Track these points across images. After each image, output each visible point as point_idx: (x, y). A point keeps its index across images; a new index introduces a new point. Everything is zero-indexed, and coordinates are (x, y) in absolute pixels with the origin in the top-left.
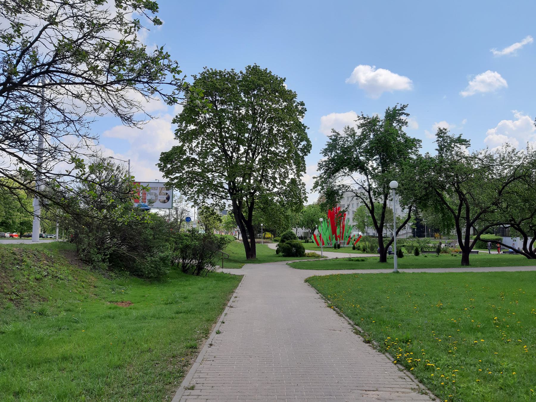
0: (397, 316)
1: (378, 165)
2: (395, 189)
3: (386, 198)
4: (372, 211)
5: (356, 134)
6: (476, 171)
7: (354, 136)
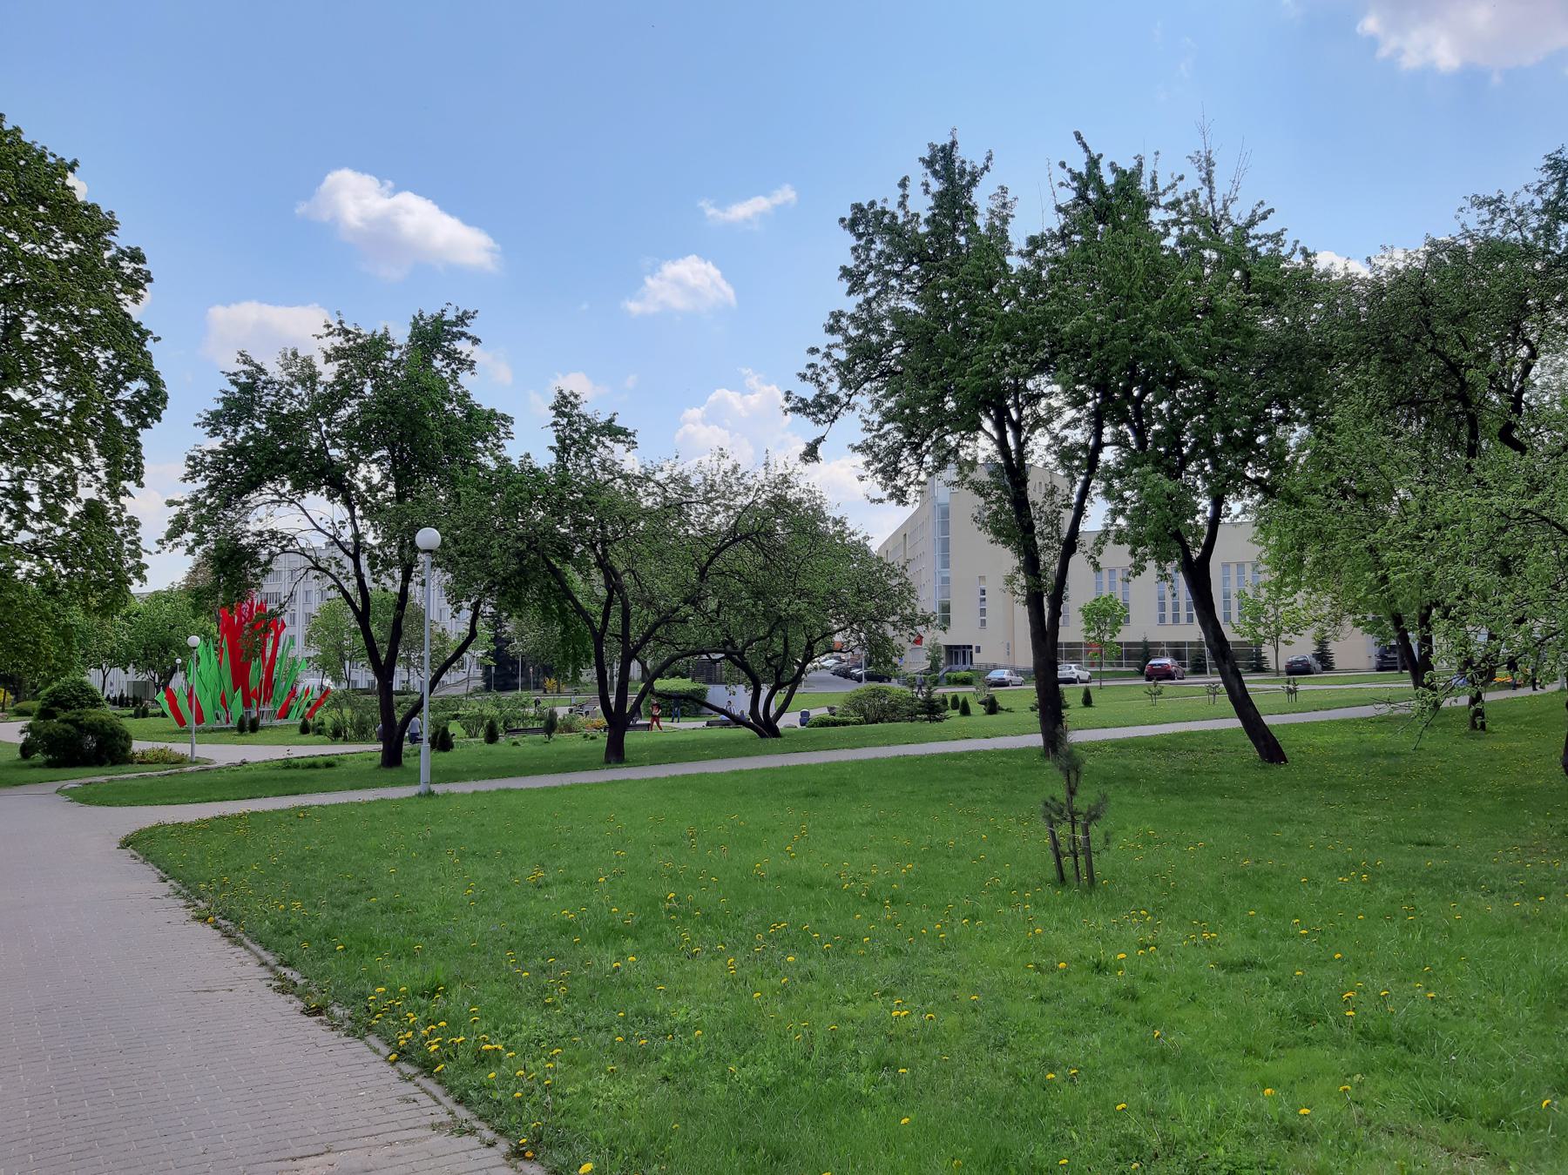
0: (415, 922)
1: (386, 476)
2: (430, 551)
3: (407, 578)
4: (363, 617)
5: (321, 378)
6: (647, 513)
7: (314, 384)
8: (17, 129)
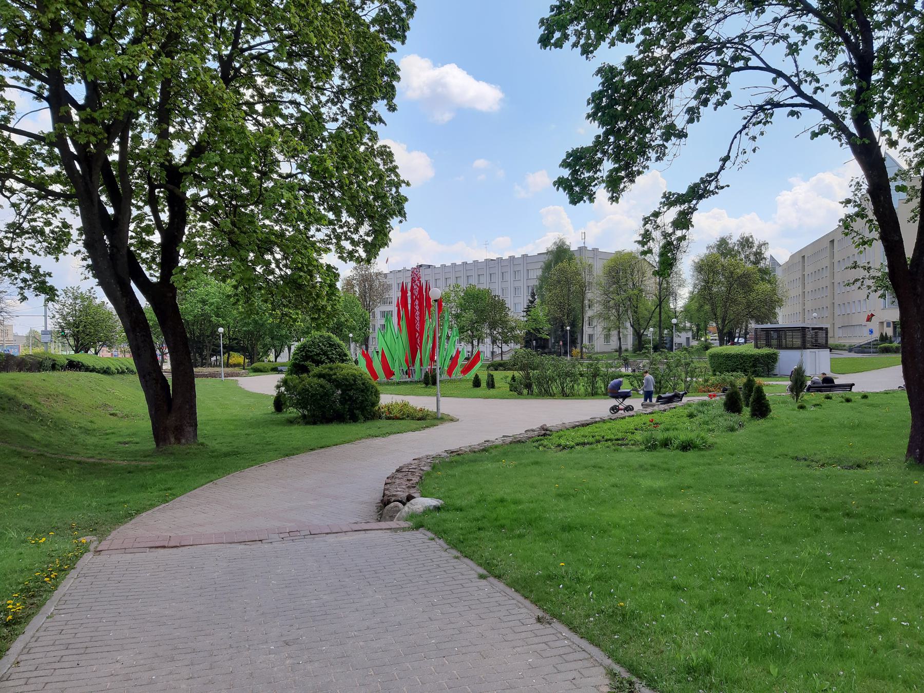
8: (542, 22)
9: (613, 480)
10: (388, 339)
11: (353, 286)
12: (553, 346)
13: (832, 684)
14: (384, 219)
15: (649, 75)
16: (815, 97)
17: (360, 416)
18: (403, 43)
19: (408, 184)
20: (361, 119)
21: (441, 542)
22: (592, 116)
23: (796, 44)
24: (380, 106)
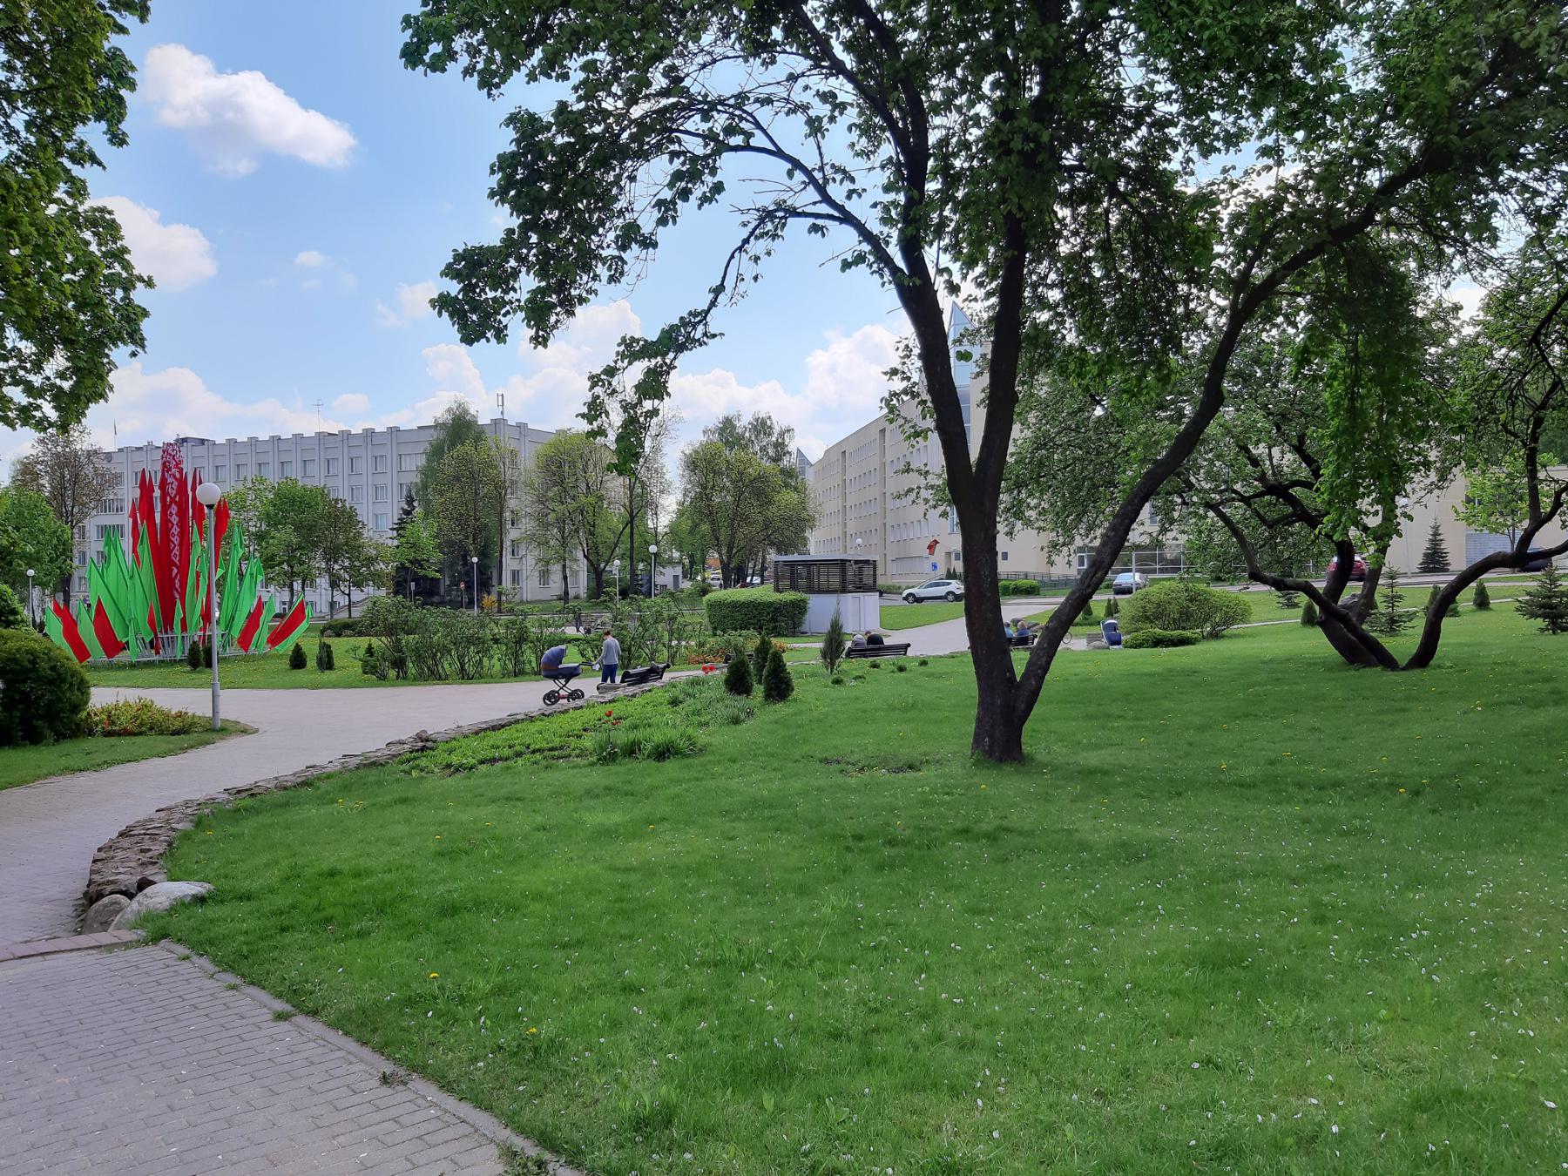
9: (539, 819)
10: (113, 576)
11: (36, 476)
12: (449, 591)
13: (853, 1111)
14: (97, 347)
15: (595, 137)
16: (849, 206)
17: (47, 732)
18: (143, 19)
19: (149, 283)
20: (51, 152)
21: (204, 962)
22: (500, 194)
23: (819, 119)
24: (92, 133)
